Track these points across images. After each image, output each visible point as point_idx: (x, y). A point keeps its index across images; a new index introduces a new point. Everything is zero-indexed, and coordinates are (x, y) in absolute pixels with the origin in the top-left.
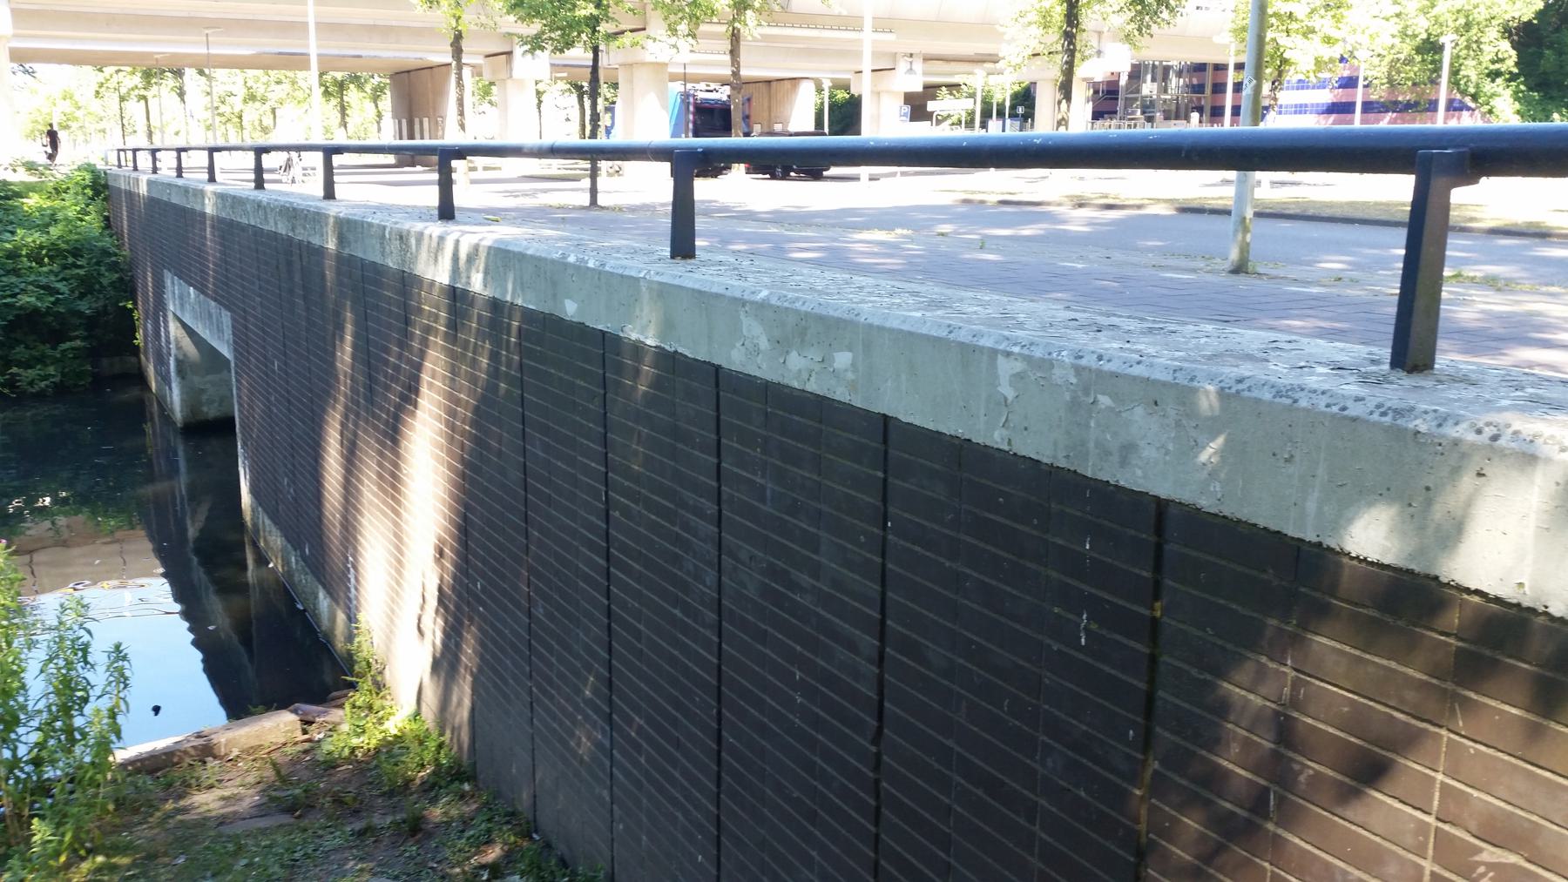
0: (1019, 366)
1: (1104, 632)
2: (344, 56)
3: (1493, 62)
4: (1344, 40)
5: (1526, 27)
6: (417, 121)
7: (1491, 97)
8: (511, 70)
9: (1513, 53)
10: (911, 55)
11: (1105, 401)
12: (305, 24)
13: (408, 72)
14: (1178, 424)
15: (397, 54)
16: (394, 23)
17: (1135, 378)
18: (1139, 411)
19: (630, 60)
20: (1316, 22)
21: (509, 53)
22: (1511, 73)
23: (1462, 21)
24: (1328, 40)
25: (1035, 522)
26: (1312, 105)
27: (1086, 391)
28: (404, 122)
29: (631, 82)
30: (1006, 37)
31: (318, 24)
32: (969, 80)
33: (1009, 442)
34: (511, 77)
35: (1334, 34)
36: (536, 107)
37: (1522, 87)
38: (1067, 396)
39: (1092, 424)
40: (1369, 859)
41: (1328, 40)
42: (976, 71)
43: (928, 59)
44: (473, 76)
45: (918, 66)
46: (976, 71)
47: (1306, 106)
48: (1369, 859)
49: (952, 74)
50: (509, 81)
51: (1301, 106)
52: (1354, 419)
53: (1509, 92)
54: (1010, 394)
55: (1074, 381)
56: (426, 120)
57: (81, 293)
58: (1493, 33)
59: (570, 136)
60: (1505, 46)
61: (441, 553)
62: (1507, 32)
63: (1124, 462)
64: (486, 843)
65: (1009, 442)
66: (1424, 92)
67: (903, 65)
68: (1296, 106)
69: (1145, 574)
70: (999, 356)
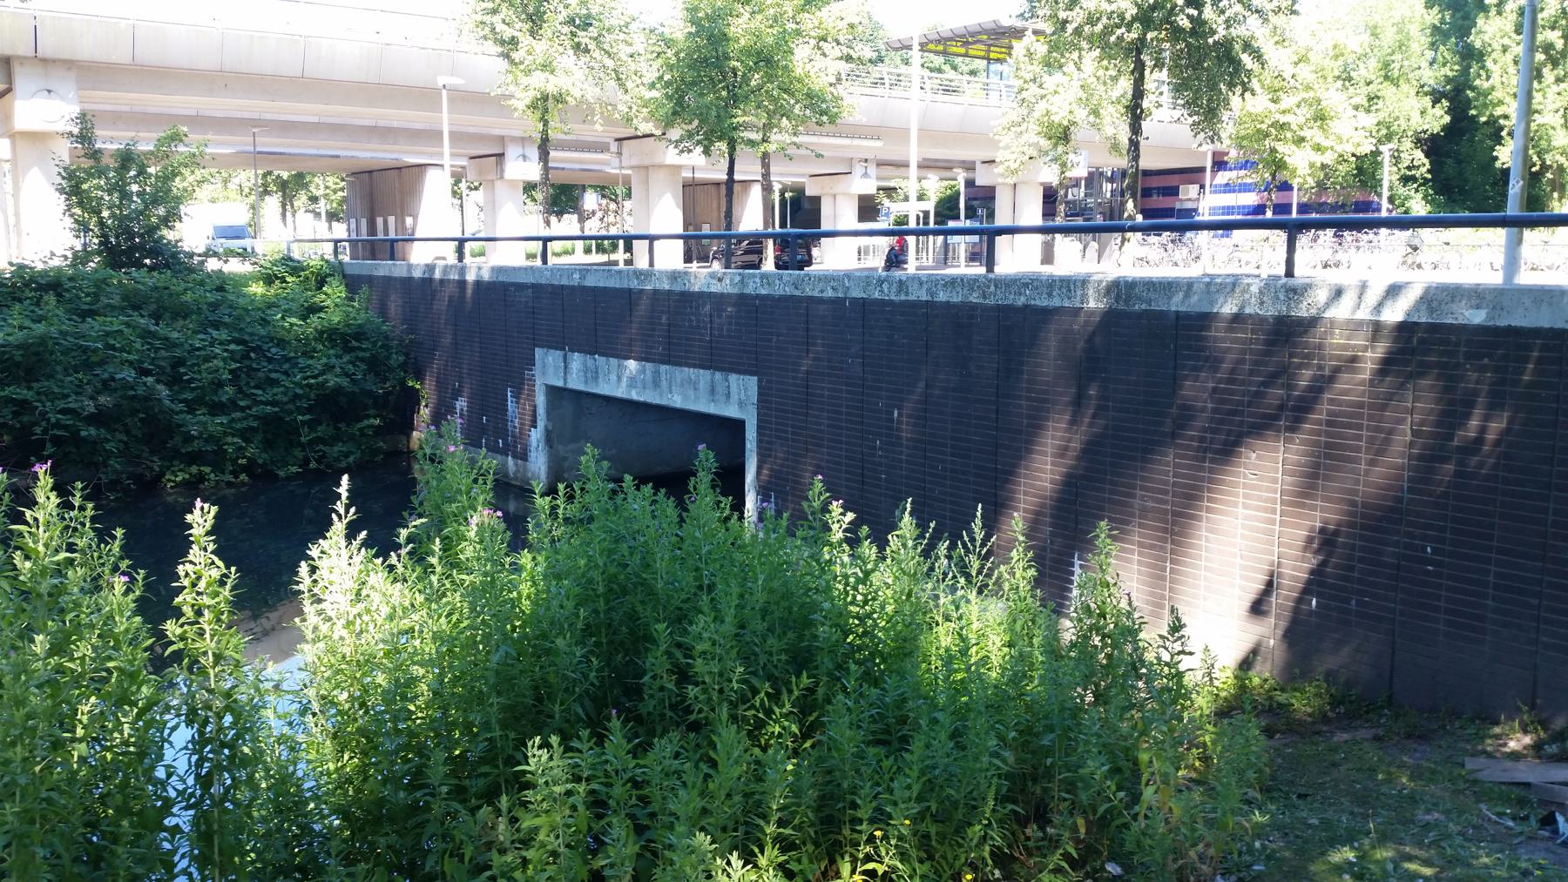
2: (322, 156)
3: (1409, 168)
4: (1332, 148)
5: (1434, 137)
6: (380, 221)
7: (1406, 199)
8: (502, 171)
9: (1426, 161)
10: (866, 161)
12: (439, 134)
13: (371, 172)
15: (374, 155)
16: (395, 124)
19: (646, 162)
20: (1306, 133)
21: (501, 156)
22: (1425, 179)
23: (1384, 132)
24: (1318, 148)
26: (1239, 207)
28: (364, 222)
29: (646, 182)
30: (1001, 145)
31: (453, 135)
32: (903, 184)
34: (502, 177)
35: (1325, 143)
36: (279, 217)
37: (1431, 192)
41: (1318, 148)
42: (929, 176)
43: (880, 164)
45: (872, 170)
46: (929, 176)
47: (1233, 207)
49: (888, 179)
50: (498, 184)
51: (1228, 207)
53: (1420, 196)
56: (391, 219)
58: (1407, 144)
59: (578, 233)
60: (1419, 155)
61: (266, 633)
62: (1418, 142)
64: (1217, 452)
66: (1349, 194)
67: (858, 170)
68: (1224, 208)
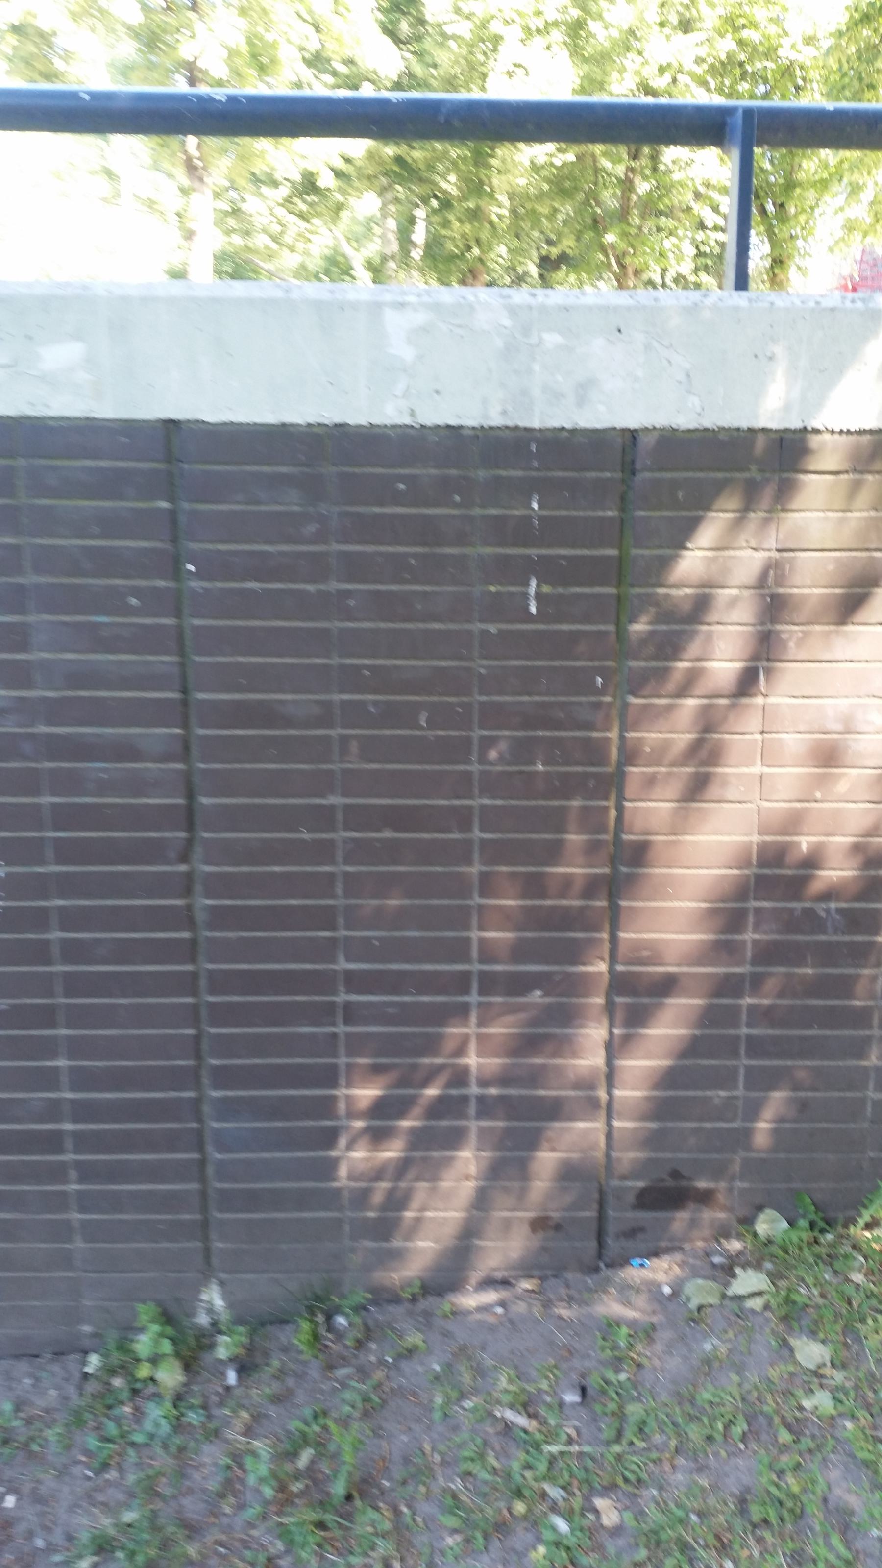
0: (420, 318)
1: (560, 590)
11: (552, 339)
14: (648, 347)
17: (590, 308)
18: (598, 344)
25: (457, 498)
27: (526, 331)
33: (413, 413)
38: (499, 343)
39: (537, 367)
40: (77, 3)
44: (448, 284)
48: (77, 3)
52: (833, 310)
54: (407, 354)
55: (507, 322)
57: (303, 267)
63: (581, 401)
65: (413, 413)
69: (610, 513)
70: (730, 1292)
